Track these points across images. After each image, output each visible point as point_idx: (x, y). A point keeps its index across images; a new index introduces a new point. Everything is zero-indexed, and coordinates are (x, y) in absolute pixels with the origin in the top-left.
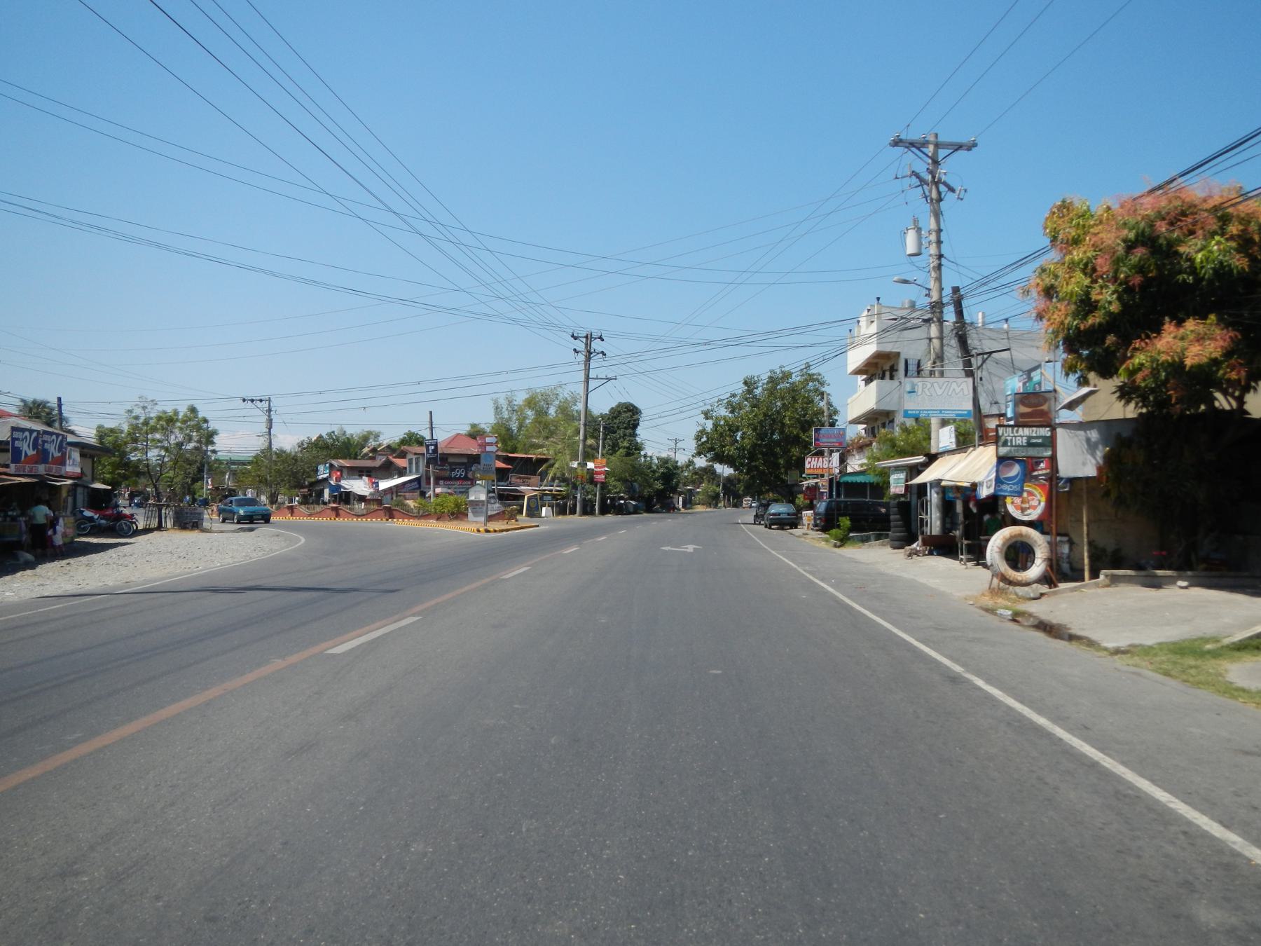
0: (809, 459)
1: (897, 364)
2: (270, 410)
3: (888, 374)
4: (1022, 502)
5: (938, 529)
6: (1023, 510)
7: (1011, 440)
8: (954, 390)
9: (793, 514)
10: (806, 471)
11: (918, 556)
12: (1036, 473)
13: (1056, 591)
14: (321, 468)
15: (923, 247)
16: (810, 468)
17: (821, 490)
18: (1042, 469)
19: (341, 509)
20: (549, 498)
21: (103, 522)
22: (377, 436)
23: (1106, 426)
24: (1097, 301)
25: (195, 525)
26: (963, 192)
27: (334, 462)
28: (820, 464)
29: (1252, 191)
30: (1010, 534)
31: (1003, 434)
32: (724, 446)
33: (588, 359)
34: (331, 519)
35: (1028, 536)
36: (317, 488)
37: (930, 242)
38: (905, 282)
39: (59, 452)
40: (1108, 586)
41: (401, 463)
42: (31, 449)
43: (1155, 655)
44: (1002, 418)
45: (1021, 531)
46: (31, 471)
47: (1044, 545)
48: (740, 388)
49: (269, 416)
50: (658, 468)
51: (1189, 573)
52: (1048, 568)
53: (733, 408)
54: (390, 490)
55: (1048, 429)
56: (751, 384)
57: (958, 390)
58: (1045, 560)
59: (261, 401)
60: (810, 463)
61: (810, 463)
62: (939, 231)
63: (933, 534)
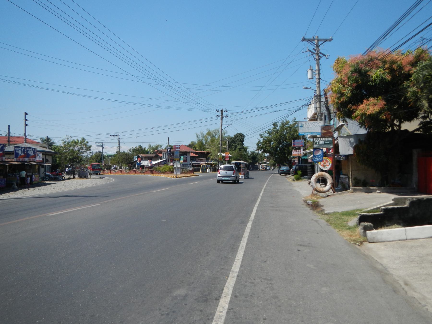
0: (293, 151)
2: (119, 139)
4: (324, 164)
6: (324, 166)
7: (318, 142)
8: (316, 125)
9: (288, 170)
10: (293, 155)
12: (329, 154)
13: (335, 194)
14: (135, 157)
15: (314, 76)
16: (294, 154)
17: (295, 162)
18: (331, 152)
20: (209, 166)
21: (53, 176)
22: (161, 146)
23: (357, 136)
24: (344, 93)
25: (85, 177)
26: (328, 56)
27: (140, 155)
29: (392, 50)
30: (318, 175)
31: (315, 140)
33: (222, 119)
34: (133, 174)
35: (324, 175)
36: (134, 164)
37: (316, 74)
38: (307, 88)
39: (33, 154)
40: (352, 192)
41: (161, 155)
42: (19, 154)
43: (332, 215)
45: (322, 174)
46: (22, 160)
47: (330, 179)
49: (119, 140)
50: (250, 155)
51: (382, 188)
52: (332, 187)
53: (270, 134)
54: (156, 164)
55: (331, 138)
57: (318, 125)
58: (331, 184)
59: (116, 135)
61: (294, 152)
62: (319, 70)
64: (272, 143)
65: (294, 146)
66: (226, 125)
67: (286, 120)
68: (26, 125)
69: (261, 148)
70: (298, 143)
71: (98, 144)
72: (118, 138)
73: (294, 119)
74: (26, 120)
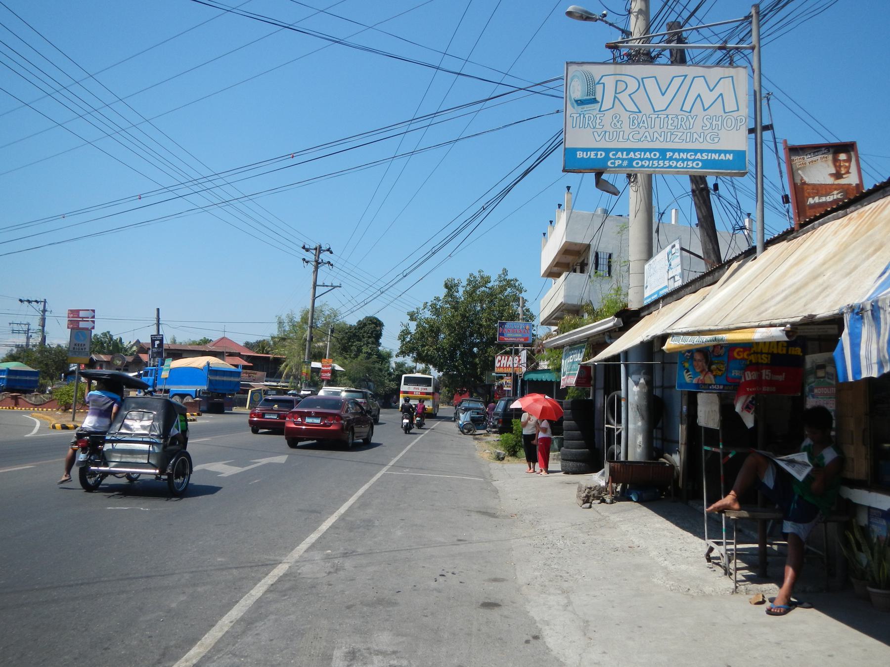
0: (499, 358)
2: (44, 311)
5: (639, 450)
10: (496, 370)
11: (603, 501)
16: (500, 367)
17: (504, 389)
19: (20, 398)
28: (510, 363)
32: (425, 346)
33: (317, 268)
34: (9, 408)
38: (586, 17)
44: (843, 156)
48: (442, 292)
49: (44, 315)
53: (436, 311)
56: (452, 287)
57: (709, 98)
59: (37, 302)
61: (499, 361)
63: (630, 459)
66: (327, 286)
69: (412, 350)
70: (514, 331)
71: (16, 327)
72: (41, 306)
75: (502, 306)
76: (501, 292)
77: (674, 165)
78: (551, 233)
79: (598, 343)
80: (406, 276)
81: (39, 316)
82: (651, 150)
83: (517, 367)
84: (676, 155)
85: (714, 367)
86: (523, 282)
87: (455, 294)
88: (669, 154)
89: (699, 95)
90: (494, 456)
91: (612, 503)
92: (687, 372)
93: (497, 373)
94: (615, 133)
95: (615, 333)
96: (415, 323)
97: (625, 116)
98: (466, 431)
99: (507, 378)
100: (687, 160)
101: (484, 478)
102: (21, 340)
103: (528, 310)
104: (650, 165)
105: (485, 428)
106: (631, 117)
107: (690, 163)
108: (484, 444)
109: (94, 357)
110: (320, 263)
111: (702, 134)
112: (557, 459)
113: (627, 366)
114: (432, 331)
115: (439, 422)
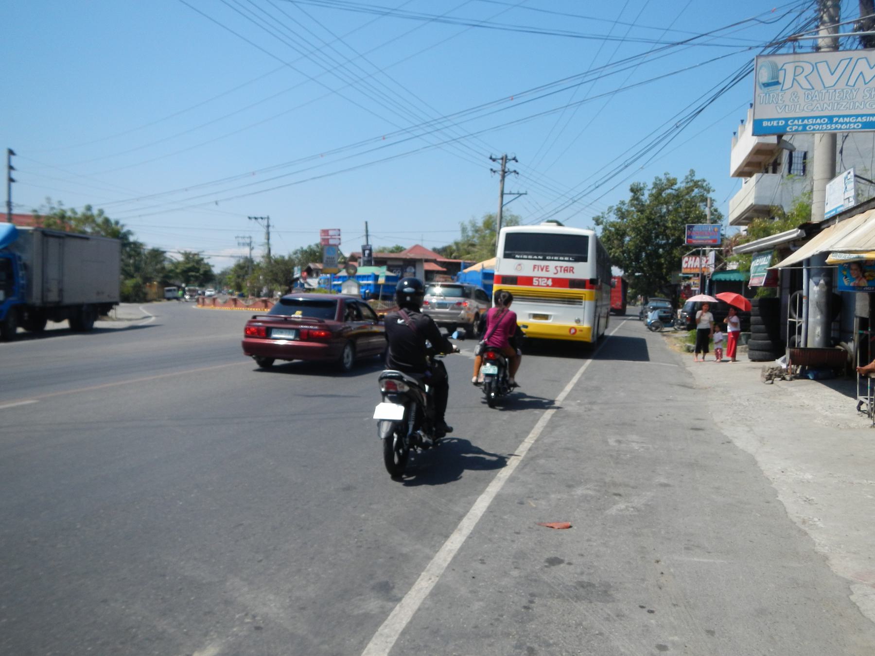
0: (686, 259)
1: (781, 158)
2: (268, 226)
3: (770, 169)
5: (817, 339)
9: (798, 345)
10: (683, 271)
11: (784, 379)
14: (296, 269)
16: (687, 268)
17: (692, 289)
28: (697, 264)
32: (611, 249)
33: (503, 177)
48: (628, 196)
53: (622, 215)
59: (262, 218)
60: (687, 262)
61: (687, 262)
63: (809, 346)
64: (627, 239)
65: (691, 242)
66: (514, 194)
67: (668, 176)
68: (11, 180)
70: (702, 233)
71: (241, 241)
72: (265, 222)
73: (691, 175)
74: (11, 168)
75: (689, 207)
76: (688, 193)
77: (839, 128)
78: (742, 132)
79: (784, 250)
80: (597, 187)
81: (264, 230)
82: (821, 117)
83: (705, 267)
84: (841, 120)
85: (867, 274)
86: (712, 181)
87: (641, 197)
88: (835, 120)
89: (861, 73)
90: (684, 349)
91: (791, 380)
92: (845, 278)
93: (684, 274)
94: (793, 107)
95: (798, 243)
96: (601, 227)
97: (801, 93)
98: (654, 328)
99: (695, 278)
100: (850, 123)
101: (678, 364)
102: (245, 252)
103: (716, 210)
104: (820, 128)
105: (672, 326)
106: (806, 93)
107: (852, 125)
108: (673, 340)
109: (312, 266)
110: (506, 173)
111: (863, 103)
112: (745, 351)
113: (809, 271)
114: (617, 234)
115: (625, 321)
